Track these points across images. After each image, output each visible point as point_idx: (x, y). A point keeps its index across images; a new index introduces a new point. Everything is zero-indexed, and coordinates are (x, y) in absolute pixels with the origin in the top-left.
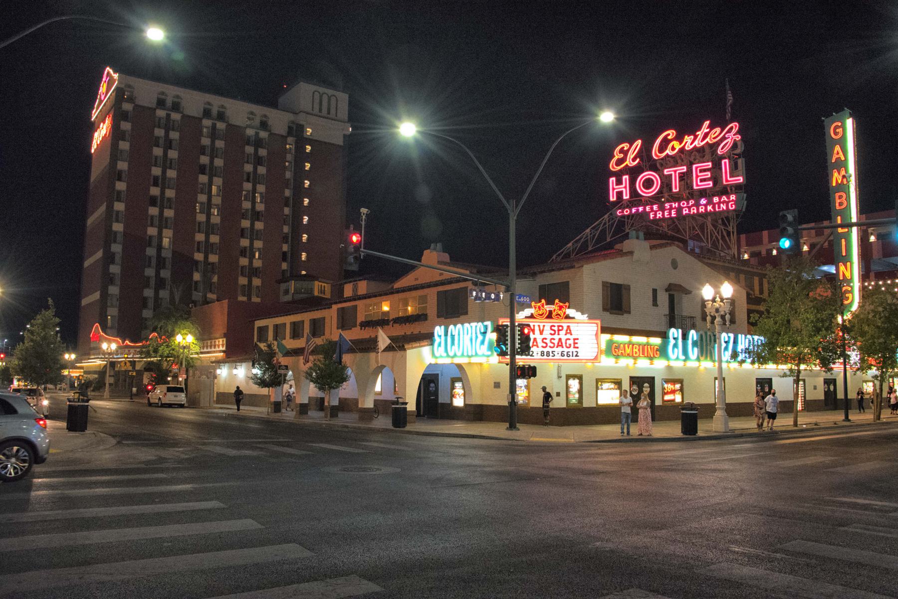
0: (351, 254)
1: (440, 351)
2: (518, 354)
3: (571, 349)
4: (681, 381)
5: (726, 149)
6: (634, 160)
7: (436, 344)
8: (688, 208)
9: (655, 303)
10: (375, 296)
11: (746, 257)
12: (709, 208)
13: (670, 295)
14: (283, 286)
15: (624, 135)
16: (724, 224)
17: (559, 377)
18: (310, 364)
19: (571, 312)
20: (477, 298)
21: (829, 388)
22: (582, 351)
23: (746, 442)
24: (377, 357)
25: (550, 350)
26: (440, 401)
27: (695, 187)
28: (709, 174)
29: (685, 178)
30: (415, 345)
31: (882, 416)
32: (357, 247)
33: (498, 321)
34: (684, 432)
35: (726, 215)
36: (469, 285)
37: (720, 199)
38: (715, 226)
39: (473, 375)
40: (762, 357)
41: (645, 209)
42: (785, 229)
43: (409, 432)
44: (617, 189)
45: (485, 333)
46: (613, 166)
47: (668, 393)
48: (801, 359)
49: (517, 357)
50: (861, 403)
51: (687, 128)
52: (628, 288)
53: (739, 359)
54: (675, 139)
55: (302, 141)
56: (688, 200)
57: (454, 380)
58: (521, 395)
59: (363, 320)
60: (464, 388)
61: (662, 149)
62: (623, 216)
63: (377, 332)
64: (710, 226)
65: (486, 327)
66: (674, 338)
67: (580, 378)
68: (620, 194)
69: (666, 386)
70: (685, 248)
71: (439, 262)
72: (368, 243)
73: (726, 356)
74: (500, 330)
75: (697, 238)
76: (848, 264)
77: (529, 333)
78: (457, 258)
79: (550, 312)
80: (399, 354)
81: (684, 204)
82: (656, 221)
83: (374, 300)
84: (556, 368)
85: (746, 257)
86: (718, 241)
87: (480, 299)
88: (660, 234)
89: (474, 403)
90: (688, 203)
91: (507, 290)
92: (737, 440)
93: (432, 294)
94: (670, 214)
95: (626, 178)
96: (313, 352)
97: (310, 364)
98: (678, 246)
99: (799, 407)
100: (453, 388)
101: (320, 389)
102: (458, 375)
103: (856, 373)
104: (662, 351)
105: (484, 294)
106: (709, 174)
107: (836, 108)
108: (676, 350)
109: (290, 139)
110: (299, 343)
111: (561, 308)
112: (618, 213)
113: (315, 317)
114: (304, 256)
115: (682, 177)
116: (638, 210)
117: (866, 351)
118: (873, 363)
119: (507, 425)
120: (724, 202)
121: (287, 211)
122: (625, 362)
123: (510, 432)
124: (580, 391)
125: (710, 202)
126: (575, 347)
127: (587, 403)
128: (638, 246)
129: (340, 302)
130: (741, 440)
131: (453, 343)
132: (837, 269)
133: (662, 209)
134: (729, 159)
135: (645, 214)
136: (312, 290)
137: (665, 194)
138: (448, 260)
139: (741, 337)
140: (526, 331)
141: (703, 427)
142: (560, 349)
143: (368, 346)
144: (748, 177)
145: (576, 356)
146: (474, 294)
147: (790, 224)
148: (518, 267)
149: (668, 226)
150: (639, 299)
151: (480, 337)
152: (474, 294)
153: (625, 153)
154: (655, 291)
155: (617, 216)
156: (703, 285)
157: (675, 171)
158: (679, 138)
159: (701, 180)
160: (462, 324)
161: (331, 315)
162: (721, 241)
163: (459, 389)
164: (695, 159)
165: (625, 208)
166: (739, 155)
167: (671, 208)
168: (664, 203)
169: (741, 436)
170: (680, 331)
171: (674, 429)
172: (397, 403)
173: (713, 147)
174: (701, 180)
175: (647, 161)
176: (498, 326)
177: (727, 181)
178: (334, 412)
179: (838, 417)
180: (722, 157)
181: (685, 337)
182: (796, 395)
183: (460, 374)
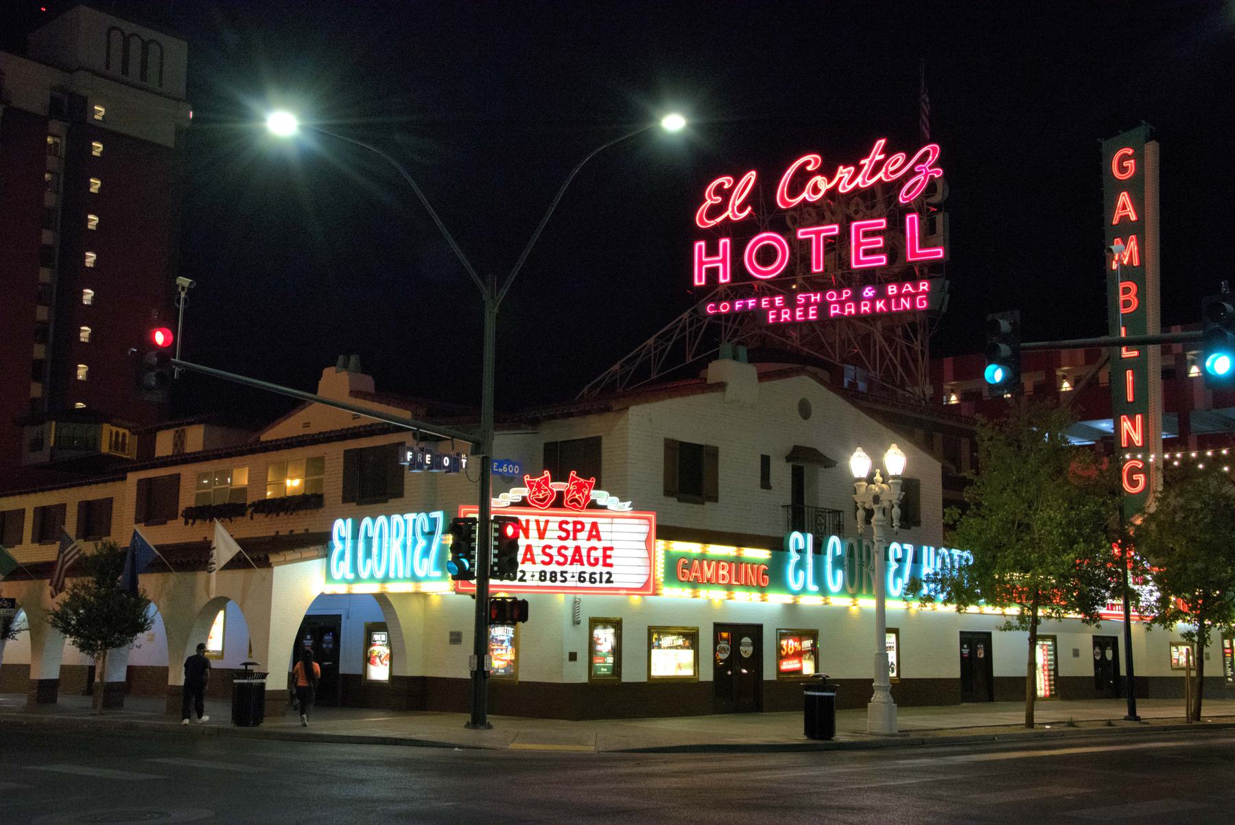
0: (151, 368)
1: (342, 569)
2: (494, 576)
3: (599, 568)
4: (813, 635)
5: (916, 194)
6: (741, 208)
7: (335, 554)
8: (840, 305)
9: (765, 483)
10: (219, 457)
11: (954, 399)
12: (880, 305)
13: (794, 469)
14: (30, 433)
15: (709, 159)
16: (907, 336)
17: (576, 622)
18: (64, 596)
19: (601, 497)
20: (415, 464)
21: (1103, 655)
22: (617, 572)
24: (208, 581)
25: (558, 569)
26: (344, 669)
27: (854, 266)
28: (880, 241)
29: (836, 246)
30: (290, 555)
31: (1203, 714)
32: (165, 354)
33: (457, 511)
34: (809, 731)
35: (910, 319)
36: (407, 438)
37: (900, 289)
38: (890, 341)
39: (409, 616)
40: (966, 592)
41: (758, 303)
42: (995, 348)
43: (267, 735)
44: (708, 263)
45: (431, 534)
46: (701, 220)
47: (788, 657)
48: (1037, 597)
49: (492, 582)
50: (1164, 688)
52: (714, 452)
53: (925, 591)
55: (83, 130)
56: (839, 289)
57: (372, 628)
58: (500, 659)
59: (192, 504)
60: (389, 644)
61: (795, 189)
62: (719, 316)
63: (212, 529)
64: (879, 337)
65: (434, 522)
66: (799, 551)
67: (617, 625)
69: (784, 643)
70: (835, 384)
71: (355, 393)
72: (190, 345)
73: (896, 587)
74: (458, 528)
75: (856, 361)
77: (516, 535)
78: (387, 385)
80: (258, 573)
81: (831, 296)
82: (778, 327)
83: (225, 463)
84: (570, 604)
85: (954, 399)
86: (895, 367)
87: (420, 466)
88: (775, 352)
89: (409, 674)
90: (840, 295)
91: (475, 452)
92: (909, 751)
93: (334, 454)
94: (806, 313)
95: (724, 242)
96: (74, 571)
97: (64, 596)
98: (814, 376)
99: (1042, 686)
100: (369, 642)
101: (83, 647)
102: (380, 618)
103: (1156, 629)
104: (774, 576)
105: (428, 457)
106: (880, 241)
107: (1117, 126)
108: (801, 573)
109: (55, 125)
110: (48, 553)
112: (709, 309)
113: (90, 498)
114: (82, 371)
117: (1167, 585)
118: (1183, 607)
119: (468, 717)
120: (908, 294)
121: (45, 275)
122: (714, 597)
123: (473, 731)
124: (617, 651)
125: (881, 294)
126: (605, 564)
127: (630, 675)
128: (734, 372)
129: (145, 468)
130: (919, 751)
131: (368, 554)
132: (1117, 427)
133: (791, 304)
134: (920, 213)
135: (759, 313)
136: (96, 441)
137: (797, 275)
138: (372, 389)
139: (927, 552)
140: (510, 531)
141: (846, 727)
142: (577, 568)
143: (194, 558)
144: (952, 250)
145: (608, 581)
146: (409, 455)
147: (1005, 338)
148: (497, 408)
149: (802, 337)
150: (735, 474)
151: (422, 542)
152: (409, 455)
153: (726, 194)
154: (765, 461)
155: (707, 316)
156: (852, 452)
157: (818, 233)
158: (828, 171)
159: (865, 251)
160: (388, 516)
161: (124, 495)
162: (900, 369)
163: (380, 647)
164: (856, 212)
165: (721, 300)
166: (938, 206)
167: (808, 303)
168: (795, 292)
169: (922, 743)
170: (810, 536)
171: (792, 728)
172: (246, 673)
173: (891, 189)
174: (865, 251)
176: (457, 520)
178: (114, 695)
179: (1117, 711)
180: (907, 209)
181: (819, 548)
182: (1032, 664)
183: (382, 614)
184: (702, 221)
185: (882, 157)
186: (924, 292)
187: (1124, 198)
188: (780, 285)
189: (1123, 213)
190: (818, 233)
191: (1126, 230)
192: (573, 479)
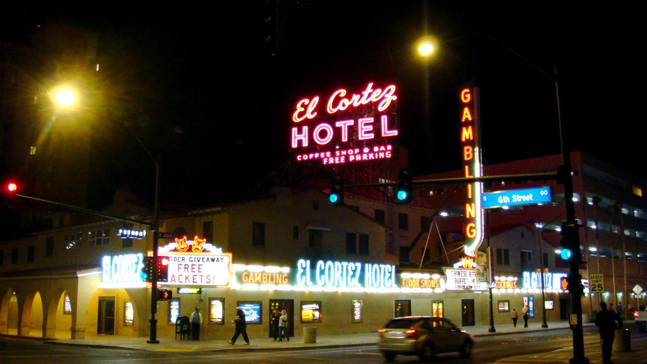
6: (312, 113)
8: (354, 155)
29: (353, 130)
41: (320, 155)
44: (299, 138)
46: (296, 118)
51: (356, 88)
54: (345, 97)
61: (335, 104)
67: (508, 301)
68: (300, 142)
76: (473, 205)
79: (191, 246)
81: (350, 152)
82: (328, 165)
94: (340, 160)
95: (305, 129)
106: (371, 128)
111: (199, 243)
115: (350, 128)
116: (314, 156)
119: (148, 339)
120: (382, 151)
125: (371, 151)
131: (116, 271)
133: (333, 155)
135: (320, 160)
151: (135, 266)
158: (349, 96)
159: (365, 131)
167: (341, 155)
170: (308, 262)
174: (365, 131)
175: (322, 115)
177: (385, 133)
184: (331, 111)
186: (389, 150)
190: (345, 124)
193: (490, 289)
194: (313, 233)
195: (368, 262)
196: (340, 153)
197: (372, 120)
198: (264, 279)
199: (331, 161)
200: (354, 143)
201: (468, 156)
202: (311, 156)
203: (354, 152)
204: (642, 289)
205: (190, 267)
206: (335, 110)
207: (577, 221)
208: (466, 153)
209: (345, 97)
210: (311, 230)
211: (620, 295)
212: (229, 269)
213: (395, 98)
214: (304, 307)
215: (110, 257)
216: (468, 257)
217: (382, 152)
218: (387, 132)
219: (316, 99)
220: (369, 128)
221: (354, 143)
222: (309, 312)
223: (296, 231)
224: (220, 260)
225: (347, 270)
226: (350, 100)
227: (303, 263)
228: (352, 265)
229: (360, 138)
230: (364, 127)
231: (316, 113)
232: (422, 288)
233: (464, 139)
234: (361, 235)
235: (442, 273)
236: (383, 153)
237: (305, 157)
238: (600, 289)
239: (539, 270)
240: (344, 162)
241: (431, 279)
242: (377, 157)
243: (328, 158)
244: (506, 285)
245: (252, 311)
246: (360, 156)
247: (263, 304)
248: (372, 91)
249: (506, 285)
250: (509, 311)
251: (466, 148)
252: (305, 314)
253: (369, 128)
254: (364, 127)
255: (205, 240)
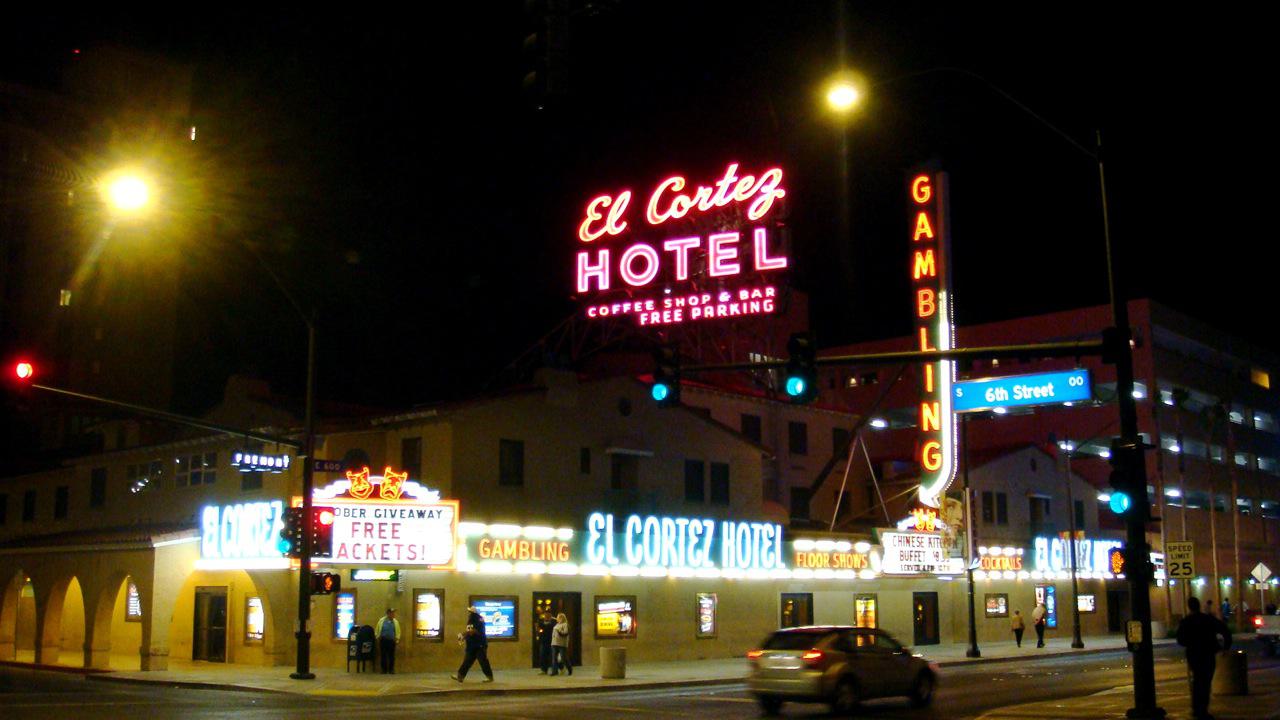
6: (618, 224)
8: (701, 308)
23: (1084, 709)
29: (698, 258)
41: (632, 307)
44: (591, 273)
46: (585, 234)
51: (704, 174)
54: (683, 192)
61: (663, 206)
67: (1005, 596)
68: (593, 281)
74: (289, 513)
76: (936, 405)
79: (377, 487)
81: (693, 300)
82: (649, 326)
94: (672, 316)
95: (604, 255)
106: (733, 253)
111: (394, 481)
115: (692, 252)
116: (621, 309)
120: (756, 299)
125: (735, 299)
131: (229, 536)
133: (659, 307)
135: (633, 316)
151: (267, 526)
158: (690, 191)
159: (721, 260)
167: (674, 307)
170: (610, 518)
174: (721, 260)
175: (638, 228)
177: (762, 264)
184: (654, 219)
185: (735, 179)
186: (770, 297)
187: (922, 218)
188: (653, 291)
189: (923, 231)
190: (682, 246)
191: (924, 244)
192: (388, 474)
193: (970, 571)
194: (619, 461)
195: (729, 519)
196: (674, 303)
197: (735, 237)
198: (522, 553)
199: (655, 318)
200: (701, 282)
201: (926, 308)
202: (615, 309)
203: (700, 301)
204: (1270, 573)
205: (376, 528)
206: (663, 218)
207: (1141, 436)
208: (922, 303)
209: (683, 192)
210: (615, 456)
211: (1226, 583)
212: (453, 532)
213: (781, 194)
214: (601, 606)
215: (217, 509)
216: (925, 508)
217: (755, 300)
218: (765, 261)
219: (626, 196)
220: (731, 254)
221: (701, 282)
222: (611, 617)
223: (586, 457)
224: (435, 514)
225: (687, 535)
226: (692, 199)
227: (599, 521)
228: (696, 524)
229: (713, 274)
230: (719, 251)
231: (624, 224)
232: (835, 569)
233: (917, 276)
234: (714, 466)
235: (875, 541)
236: (758, 303)
237: (604, 311)
238: (1187, 571)
239: (1067, 534)
240: (680, 320)
241: (852, 552)
242: (745, 311)
243: (649, 312)
244: (1001, 563)
245: (498, 615)
246: (711, 308)
247: (520, 602)
248: (735, 179)
249: (1001, 563)
250: (1006, 615)
251: (922, 293)
252: (604, 622)
253: (731, 254)
254: (719, 251)
255: (405, 475)
